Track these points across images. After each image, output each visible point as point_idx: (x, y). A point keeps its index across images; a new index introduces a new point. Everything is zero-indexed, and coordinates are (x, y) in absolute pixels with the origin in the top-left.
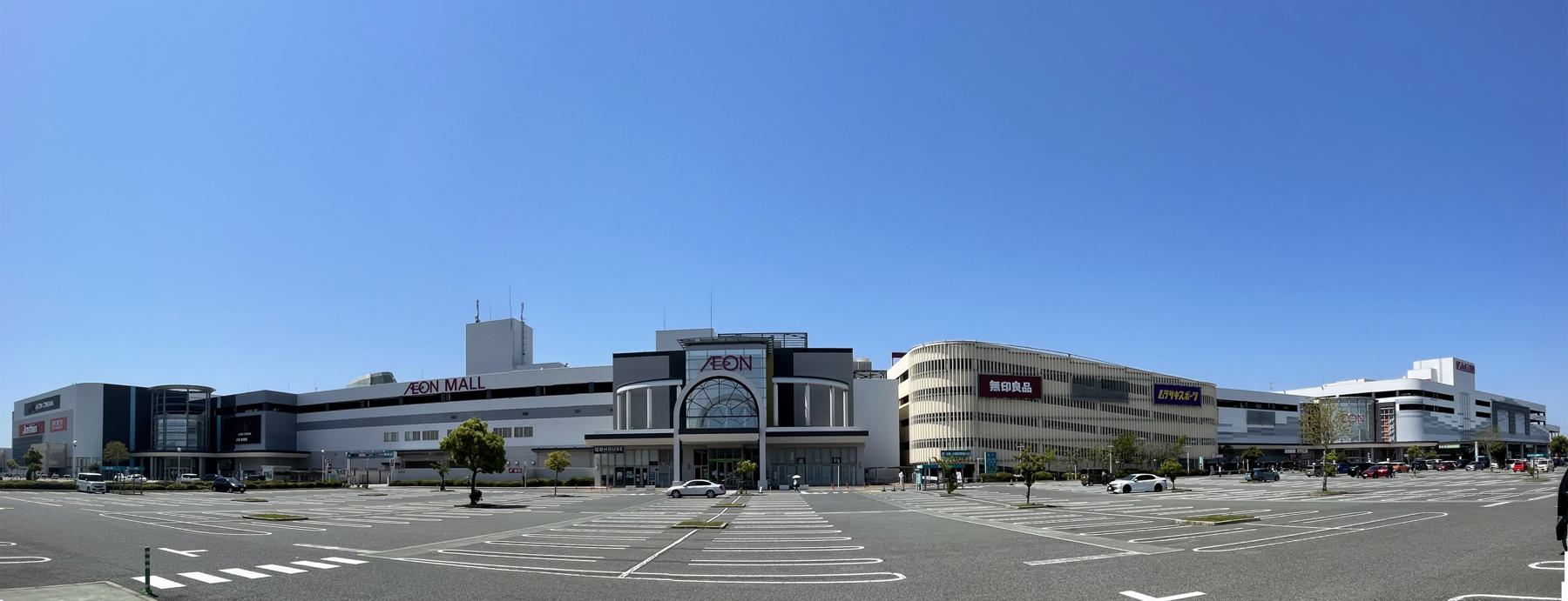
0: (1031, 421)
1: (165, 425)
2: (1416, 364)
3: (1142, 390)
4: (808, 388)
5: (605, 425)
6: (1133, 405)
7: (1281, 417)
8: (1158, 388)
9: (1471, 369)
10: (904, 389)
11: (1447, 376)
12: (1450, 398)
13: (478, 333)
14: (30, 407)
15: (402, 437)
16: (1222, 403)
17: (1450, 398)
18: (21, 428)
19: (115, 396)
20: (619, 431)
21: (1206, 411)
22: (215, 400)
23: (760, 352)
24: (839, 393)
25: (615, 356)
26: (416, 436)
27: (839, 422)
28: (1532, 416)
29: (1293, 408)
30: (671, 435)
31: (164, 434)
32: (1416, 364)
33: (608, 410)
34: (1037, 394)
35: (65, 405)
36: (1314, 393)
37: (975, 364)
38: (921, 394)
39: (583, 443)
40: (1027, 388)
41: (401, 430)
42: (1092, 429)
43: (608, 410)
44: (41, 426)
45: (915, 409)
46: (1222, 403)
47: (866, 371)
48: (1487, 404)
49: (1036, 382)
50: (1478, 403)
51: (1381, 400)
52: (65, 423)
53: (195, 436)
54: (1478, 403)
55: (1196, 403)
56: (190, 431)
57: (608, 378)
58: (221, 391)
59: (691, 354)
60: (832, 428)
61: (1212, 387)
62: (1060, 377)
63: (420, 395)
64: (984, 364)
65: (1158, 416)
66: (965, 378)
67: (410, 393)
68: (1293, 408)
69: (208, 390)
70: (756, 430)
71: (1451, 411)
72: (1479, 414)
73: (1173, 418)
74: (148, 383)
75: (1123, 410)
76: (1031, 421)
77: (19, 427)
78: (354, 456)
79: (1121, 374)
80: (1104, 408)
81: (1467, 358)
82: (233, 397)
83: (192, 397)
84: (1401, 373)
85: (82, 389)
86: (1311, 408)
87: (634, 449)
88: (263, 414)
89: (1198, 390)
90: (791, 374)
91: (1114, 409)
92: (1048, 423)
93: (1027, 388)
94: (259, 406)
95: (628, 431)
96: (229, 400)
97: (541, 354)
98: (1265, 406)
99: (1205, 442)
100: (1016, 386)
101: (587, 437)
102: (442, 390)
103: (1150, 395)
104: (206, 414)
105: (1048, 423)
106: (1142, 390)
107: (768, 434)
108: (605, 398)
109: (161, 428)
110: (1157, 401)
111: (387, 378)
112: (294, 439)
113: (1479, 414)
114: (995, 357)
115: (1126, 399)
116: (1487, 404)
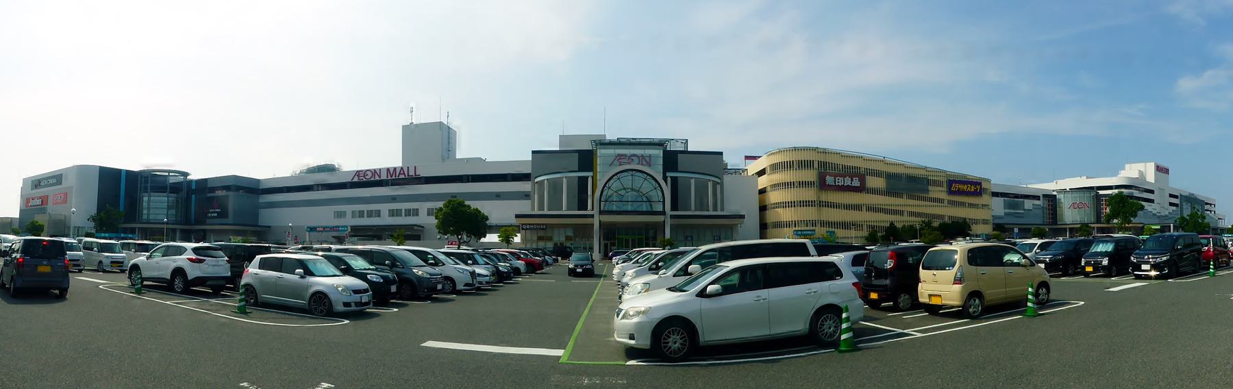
0: (858, 207)
1: (149, 201)
2: (1127, 166)
3: (939, 184)
4: (693, 181)
5: (524, 207)
6: (932, 195)
7: (1028, 204)
8: (951, 183)
9: (1166, 171)
10: (763, 182)
11: (1151, 177)
12: (1152, 192)
13: (412, 134)
14: (37, 183)
15: (349, 214)
16: (995, 194)
17: (1152, 192)
18: (28, 201)
19: (110, 180)
20: (536, 212)
21: (985, 199)
22: (191, 181)
23: (659, 152)
24: (715, 184)
25: (534, 152)
26: (361, 214)
27: (715, 209)
28: (1207, 207)
29: (1037, 198)
30: (592, 216)
31: (148, 209)
32: (1127, 166)
33: (526, 196)
34: (862, 189)
35: (65, 184)
36: (1050, 187)
37: (816, 165)
38: (776, 186)
39: (514, 221)
40: (856, 183)
41: (348, 208)
42: (901, 213)
43: (526, 196)
44: (44, 200)
45: (774, 197)
46: (995, 194)
47: (737, 171)
48: (1176, 197)
49: (862, 179)
50: (1171, 196)
51: (1101, 192)
52: (65, 198)
53: (173, 212)
54: (1171, 196)
55: (978, 193)
56: (169, 208)
57: (528, 170)
58: (195, 176)
59: (601, 152)
60: (712, 213)
61: (988, 181)
62: (877, 174)
63: (364, 180)
64: (823, 165)
65: (951, 203)
66: (810, 175)
67: (356, 179)
68: (1037, 198)
69: (185, 174)
70: (663, 213)
71: (1152, 201)
72: (1171, 204)
73: (962, 204)
74: (136, 167)
75: (924, 199)
76: (858, 207)
77: (26, 200)
78: (312, 229)
79: (923, 172)
80: (911, 197)
81: (1164, 164)
82: (206, 180)
83: (172, 180)
84: (1115, 174)
85: (82, 170)
86: (1051, 199)
87: (552, 226)
88: (231, 194)
89: (980, 184)
90: (677, 171)
91: (919, 198)
92: (871, 209)
93: (829, 180)
94: (227, 188)
95: (546, 212)
96: (203, 183)
97: (464, 150)
98: (1017, 196)
99: (985, 222)
100: (848, 182)
101: (517, 216)
102: (384, 177)
103: (945, 189)
104: (184, 194)
105: (871, 209)
106: (939, 184)
107: (672, 217)
108: (525, 186)
109: (145, 204)
110: (950, 192)
111: (329, 169)
112: (256, 215)
113: (1171, 204)
114: (829, 159)
115: (927, 191)
116: (1176, 197)
